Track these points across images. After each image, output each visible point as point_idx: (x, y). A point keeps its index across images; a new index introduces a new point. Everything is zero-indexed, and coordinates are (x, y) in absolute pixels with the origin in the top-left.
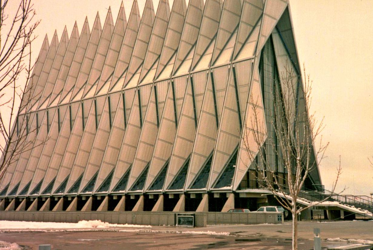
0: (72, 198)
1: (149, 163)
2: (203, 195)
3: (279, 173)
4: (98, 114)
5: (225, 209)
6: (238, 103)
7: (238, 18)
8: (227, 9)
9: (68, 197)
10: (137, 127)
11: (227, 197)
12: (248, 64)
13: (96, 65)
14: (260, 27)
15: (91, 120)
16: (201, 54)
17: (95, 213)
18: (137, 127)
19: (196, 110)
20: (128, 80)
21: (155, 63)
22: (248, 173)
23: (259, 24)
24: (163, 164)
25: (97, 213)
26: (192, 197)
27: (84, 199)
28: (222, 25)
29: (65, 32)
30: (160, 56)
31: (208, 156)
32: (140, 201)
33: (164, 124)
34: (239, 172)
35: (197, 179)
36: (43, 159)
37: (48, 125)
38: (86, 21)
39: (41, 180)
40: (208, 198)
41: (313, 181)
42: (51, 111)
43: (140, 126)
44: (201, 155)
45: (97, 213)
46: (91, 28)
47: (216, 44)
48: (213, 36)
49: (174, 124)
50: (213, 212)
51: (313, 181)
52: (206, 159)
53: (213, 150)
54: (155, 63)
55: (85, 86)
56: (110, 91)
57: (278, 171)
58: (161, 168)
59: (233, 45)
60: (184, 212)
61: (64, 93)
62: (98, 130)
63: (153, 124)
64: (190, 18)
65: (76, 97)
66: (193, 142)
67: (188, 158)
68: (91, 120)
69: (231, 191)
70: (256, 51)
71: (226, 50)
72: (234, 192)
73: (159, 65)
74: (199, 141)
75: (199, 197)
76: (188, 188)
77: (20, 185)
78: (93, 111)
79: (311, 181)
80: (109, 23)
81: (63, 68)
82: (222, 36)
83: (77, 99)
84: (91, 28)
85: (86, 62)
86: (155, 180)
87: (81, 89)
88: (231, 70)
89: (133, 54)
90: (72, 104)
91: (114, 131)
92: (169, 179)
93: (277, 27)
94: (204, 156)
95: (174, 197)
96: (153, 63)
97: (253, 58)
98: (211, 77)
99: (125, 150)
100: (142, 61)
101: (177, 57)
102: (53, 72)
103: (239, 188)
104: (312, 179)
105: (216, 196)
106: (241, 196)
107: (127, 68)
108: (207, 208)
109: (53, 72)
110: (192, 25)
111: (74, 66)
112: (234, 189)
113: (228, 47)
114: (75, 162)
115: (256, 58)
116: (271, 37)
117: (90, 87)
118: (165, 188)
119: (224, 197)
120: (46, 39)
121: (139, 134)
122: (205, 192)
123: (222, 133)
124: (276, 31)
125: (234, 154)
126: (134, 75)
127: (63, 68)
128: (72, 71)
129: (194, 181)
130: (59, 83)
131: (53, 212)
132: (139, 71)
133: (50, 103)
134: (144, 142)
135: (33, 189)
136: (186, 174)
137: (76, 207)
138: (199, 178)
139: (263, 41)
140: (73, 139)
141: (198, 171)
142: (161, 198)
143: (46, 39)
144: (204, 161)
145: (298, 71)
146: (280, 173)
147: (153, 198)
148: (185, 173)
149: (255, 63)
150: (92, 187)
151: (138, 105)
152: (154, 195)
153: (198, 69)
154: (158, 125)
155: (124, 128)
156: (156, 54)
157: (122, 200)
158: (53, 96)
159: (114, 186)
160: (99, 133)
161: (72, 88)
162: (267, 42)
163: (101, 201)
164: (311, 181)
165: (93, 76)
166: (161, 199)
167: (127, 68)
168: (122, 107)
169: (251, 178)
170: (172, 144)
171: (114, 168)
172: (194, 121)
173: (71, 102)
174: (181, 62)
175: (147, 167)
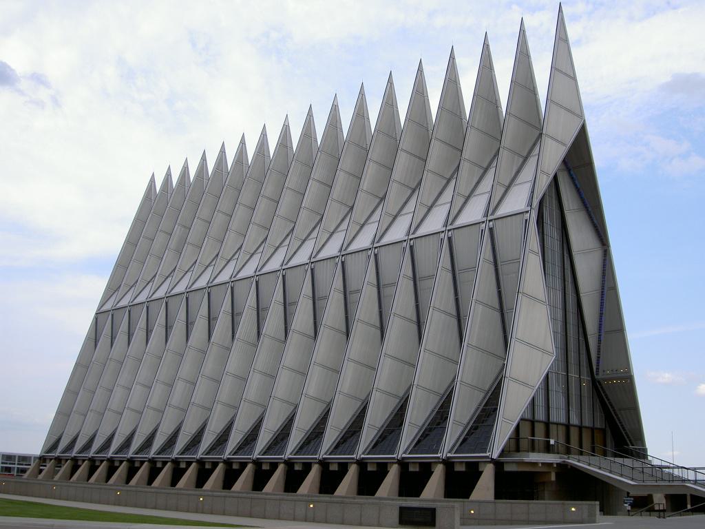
0: (187, 464)
1: (296, 407)
2: (432, 465)
3: (584, 427)
4: (350, 288)
5: (476, 495)
6: (500, 293)
7: (459, 153)
8: (476, 126)
9: (180, 462)
10: (308, 336)
11: (480, 470)
12: (434, 241)
13: (235, 224)
14: (494, 169)
15: (223, 322)
16: (429, 205)
17: (370, 501)
18: (308, 336)
19: (420, 305)
20: (385, 229)
21: (343, 220)
22: (517, 428)
23: (536, 151)
24: (357, 405)
25: (176, 491)
26: (411, 469)
27: (208, 466)
28: (466, 154)
29: (168, 175)
30: (352, 208)
31: (401, 395)
32: (314, 474)
33: (358, 330)
34: (504, 424)
35: (380, 437)
36: (137, 390)
37: (166, 326)
38: (264, 133)
39: (175, 427)
40: (397, 472)
41: (630, 440)
42: (194, 299)
43: (313, 334)
44: (430, 391)
45: (176, 491)
46: (158, 189)
47: (458, 184)
48: (416, 184)
49: (379, 332)
50: (523, 501)
51: (630, 440)
52: (439, 398)
53: (453, 380)
54: (314, 228)
55: (238, 254)
56: (259, 271)
57: (571, 422)
58: (318, 416)
59: (489, 189)
60: (397, 497)
61: (178, 274)
62: (235, 341)
63: (374, 326)
64: (375, 154)
65: (218, 278)
66: (413, 366)
67: (405, 394)
68: (223, 322)
69: (490, 460)
70: (532, 197)
71: (437, 208)
72: (493, 461)
73: (351, 224)
74: (386, 368)
75: (383, 469)
76: (405, 453)
77: (96, 438)
78: (371, 276)
79: (627, 440)
80: (421, 91)
81: (179, 229)
82: (430, 185)
83: (179, 289)
84: (158, 189)
85: (240, 213)
86: (341, 436)
87: (167, 277)
88: (487, 233)
89: (253, 220)
90: (190, 294)
91: (265, 341)
92: (367, 436)
93: (565, 162)
94: (480, 390)
95: (466, 468)
96: (474, 184)
97: (527, 212)
98: (341, 270)
99: (227, 384)
100: (319, 217)
101: (419, 200)
102: (160, 238)
103: (502, 454)
104: (628, 437)
105: (460, 468)
106: (508, 468)
107: (293, 230)
108: (442, 491)
109: (160, 238)
110: (411, 154)
111: (198, 226)
112: (495, 456)
113: (479, 190)
114: (193, 399)
115: (533, 211)
116: (555, 178)
117: (224, 263)
118: (360, 452)
119: (473, 472)
120: (152, 181)
121: (310, 352)
122: (437, 460)
123: (470, 350)
124: (564, 167)
125: (495, 385)
126: (304, 242)
127: (178, 231)
128: (193, 236)
129: (375, 441)
130: (169, 256)
131: (153, 490)
132: (314, 234)
133: (116, 302)
134: (320, 365)
135: (158, 446)
136: (401, 424)
137: (318, 484)
138: (427, 433)
139: (544, 182)
140: (190, 356)
141: (468, 418)
142: (353, 470)
143: (152, 181)
144: (393, 404)
145: (604, 240)
146: (586, 427)
147: (375, 469)
148: (399, 423)
149: (532, 218)
150: (252, 445)
151: (375, 283)
152: (304, 463)
153: (423, 231)
154: (348, 334)
155: (283, 339)
156: (443, 177)
157: (392, 477)
158: (157, 280)
159: (81, 446)
160: (237, 345)
161: (192, 266)
162: (550, 185)
163: (211, 471)
164: (627, 440)
165: (231, 241)
166: (439, 472)
167: (293, 230)
168: (410, 274)
169: (522, 435)
170: (338, 372)
171: (263, 413)
172: (415, 327)
173: (189, 290)
174: (391, 219)
175: (326, 411)
